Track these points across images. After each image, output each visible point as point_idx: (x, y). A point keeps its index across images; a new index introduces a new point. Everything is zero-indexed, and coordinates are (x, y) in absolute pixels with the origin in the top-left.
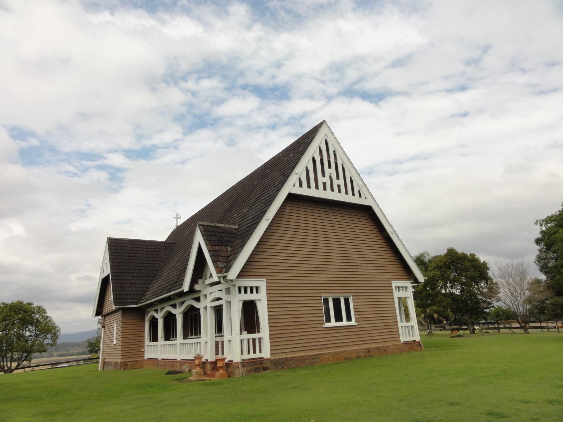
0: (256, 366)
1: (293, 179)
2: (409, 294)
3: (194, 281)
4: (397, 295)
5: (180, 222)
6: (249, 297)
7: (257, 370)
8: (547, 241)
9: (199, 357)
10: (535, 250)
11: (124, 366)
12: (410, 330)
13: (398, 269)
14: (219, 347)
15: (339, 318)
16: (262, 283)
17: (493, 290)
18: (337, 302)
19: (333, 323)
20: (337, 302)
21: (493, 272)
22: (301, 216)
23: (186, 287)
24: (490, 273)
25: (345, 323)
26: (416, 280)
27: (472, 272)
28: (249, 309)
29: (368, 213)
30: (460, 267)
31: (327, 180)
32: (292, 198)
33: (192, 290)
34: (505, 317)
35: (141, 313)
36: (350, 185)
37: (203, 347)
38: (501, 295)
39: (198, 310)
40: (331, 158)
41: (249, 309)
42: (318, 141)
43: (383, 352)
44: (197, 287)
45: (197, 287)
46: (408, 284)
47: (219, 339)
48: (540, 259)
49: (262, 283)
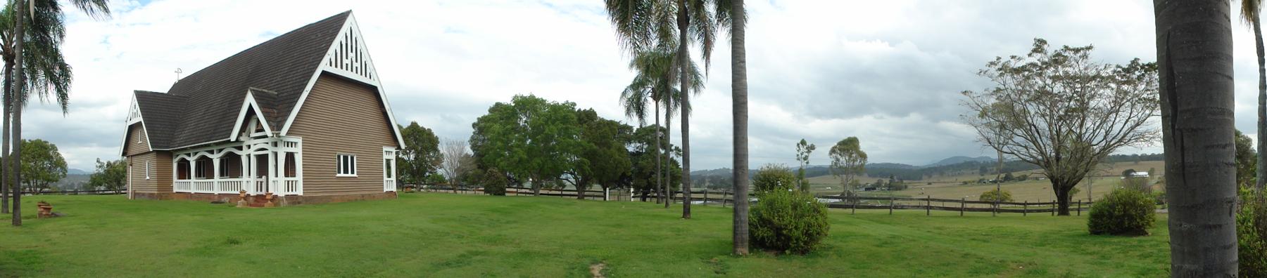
0: (293, 200)
1: (326, 60)
2: (393, 157)
3: (240, 134)
4: (385, 157)
5: (182, 77)
6: (290, 150)
7: (294, 203)
8: (482, 126)
9: (243, 192)
10: (471, 131)
11: (160, 197)
12: (390, 185)
13: (385, 134)
14: (289, 186)
15: (346, 171)
16: (299, 140)
17: (439, 159)
18: (346, 158)
19: (342, 174)
20: (346, 158)
21: (442, 148)
22: (331, 88)
23: (233, 138)
24: (439, 147)
25: (350, 175)
26: (399, 147)
27: (427, 144)
28: (290, 158)
29: (373, 91)
30: (420, 139)
31: (349, 62)
32: (324, 74)
33: (237, 140)
34: (438, 183)
35: (170, 155)
36: (364, 69)
37: (248, 183)
38: (444, 164)
39: (239, 157)
40: (352, 44)
41: (290, 158)
42: (345, 29)
43: (372, 197)
44: (242, 139)
45: (242, 139)
46: (394, 150)
47: (290, 179)
48: (473, 139)
49: (299, 140)
